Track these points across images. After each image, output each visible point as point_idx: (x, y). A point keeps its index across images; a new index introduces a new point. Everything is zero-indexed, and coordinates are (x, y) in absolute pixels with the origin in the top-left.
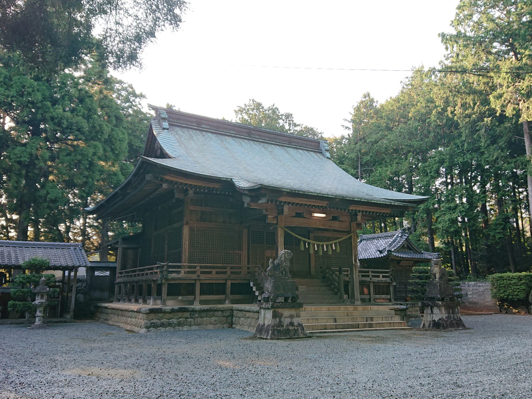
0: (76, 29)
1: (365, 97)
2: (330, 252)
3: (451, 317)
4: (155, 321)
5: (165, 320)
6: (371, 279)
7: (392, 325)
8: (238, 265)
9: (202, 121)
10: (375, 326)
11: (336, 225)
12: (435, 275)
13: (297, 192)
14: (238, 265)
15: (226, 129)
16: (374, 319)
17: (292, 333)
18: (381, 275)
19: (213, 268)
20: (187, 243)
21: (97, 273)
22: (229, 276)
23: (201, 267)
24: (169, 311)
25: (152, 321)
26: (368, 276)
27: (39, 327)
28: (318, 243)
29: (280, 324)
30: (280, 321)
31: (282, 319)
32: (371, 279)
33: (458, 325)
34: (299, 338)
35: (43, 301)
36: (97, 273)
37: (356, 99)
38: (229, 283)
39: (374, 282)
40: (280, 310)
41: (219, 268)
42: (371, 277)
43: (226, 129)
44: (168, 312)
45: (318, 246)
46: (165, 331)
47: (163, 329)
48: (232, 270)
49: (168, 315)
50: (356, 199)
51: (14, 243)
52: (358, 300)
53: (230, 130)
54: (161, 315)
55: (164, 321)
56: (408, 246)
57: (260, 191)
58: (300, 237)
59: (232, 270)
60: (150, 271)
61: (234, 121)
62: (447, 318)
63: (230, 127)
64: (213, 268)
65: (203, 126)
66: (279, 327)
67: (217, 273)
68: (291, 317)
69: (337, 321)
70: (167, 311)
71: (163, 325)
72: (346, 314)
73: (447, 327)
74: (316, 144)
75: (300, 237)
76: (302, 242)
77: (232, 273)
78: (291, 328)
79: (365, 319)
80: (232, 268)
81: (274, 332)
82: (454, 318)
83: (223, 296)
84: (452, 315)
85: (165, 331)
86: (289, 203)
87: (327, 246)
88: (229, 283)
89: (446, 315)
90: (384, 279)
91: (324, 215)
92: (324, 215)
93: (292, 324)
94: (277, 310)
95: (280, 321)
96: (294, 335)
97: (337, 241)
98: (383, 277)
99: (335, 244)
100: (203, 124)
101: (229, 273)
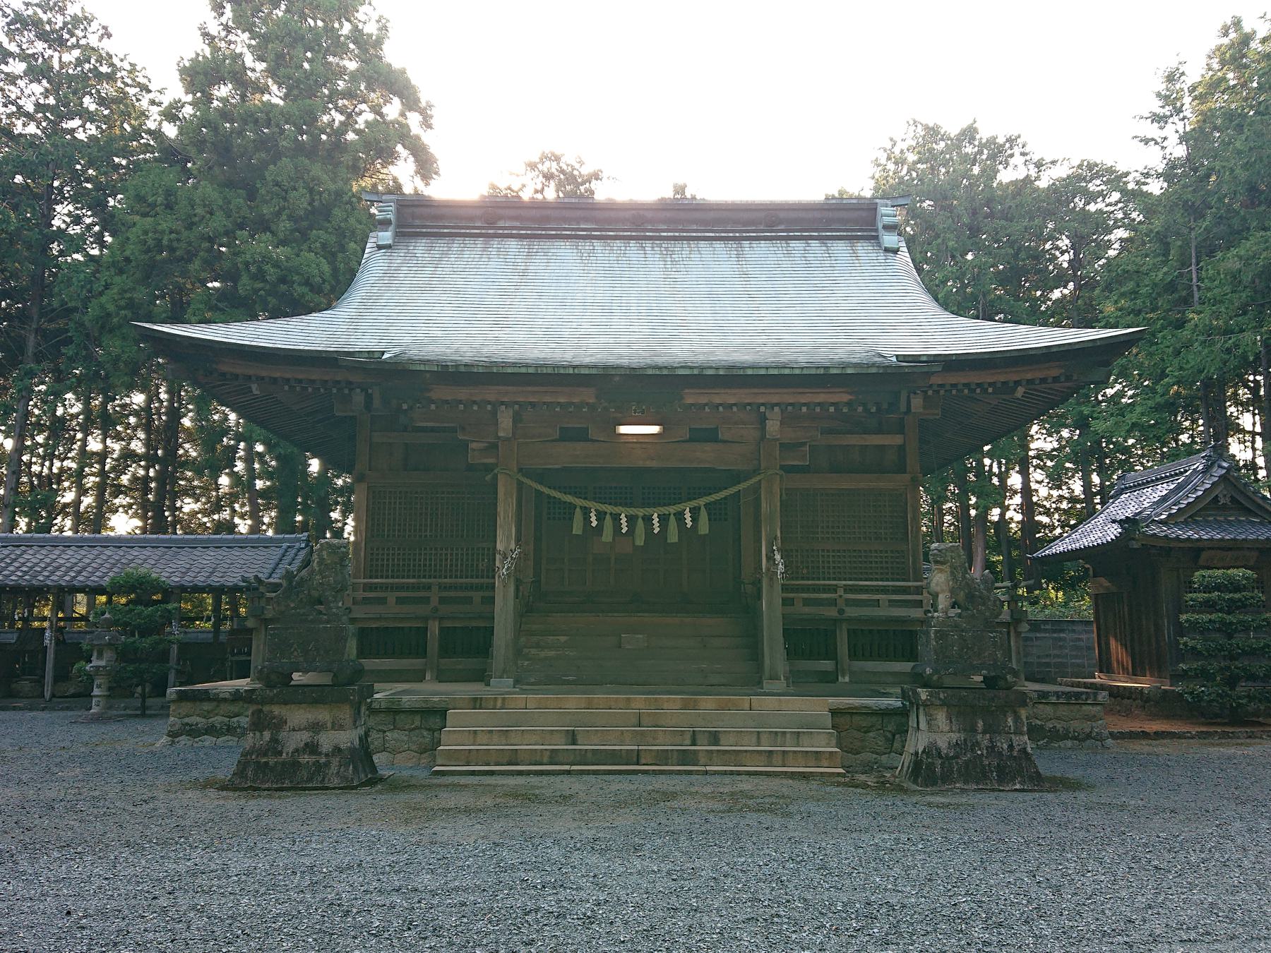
1: (1226, 34)
2: (673, 537)
4: (194, 720)
5: (220, 718)
6: (841, 612)
7: (777, 759)
8: (477, 581)
9: (501, 212)
10: (702, 761)
11: (705, 455)
12: (935, 596)
13: (462, 369)
14: (477, 581)
15: (565, 220)
17: (305, 774)
18: (392, 597)
22: (436, 610)
24: (227, 695)
25: (186, 720)
27: (99, 719)
28: (632, 511)
29: (274, 747)
30: (274, 740)
31: (283, 735)
33: (1013, 772)
34: (327, 788)
35: (102, 663)
38: (434, 628)
39: (850, 620)
40: (276, 710)
43: (565, 220)
44: (225, 700)
45: (601, 516)
46: (215, 747)
47: (208, 740)
49: (225, 708)
50: (849, 371)
51: (209, 541)
52: (774, 677)
53: (578, 221)
54: (207, 706)
55: (217, 720)
56: (1233, 499)
58: (569, 498)
59: (445, 594)
61: (526, 196)
63: (579, 213)
65: (501, 224)
66: (265, 755)
67: (400, 601)
68: (316, 727)
69: (580, 738)
70: (221, 696)
71: (211, 730)
72: (635, 721)
73: (947, 778)
74: (864, 214)
75: (569, 498)
76: (578, 509)
77: (443, 600)
78: (305, 759)
80: (443, 587)
81: (244, 769)
83: (416, 663)
84: (984, 740)
85: (215, 747)
86: (533, 405)
87: (631, 520)
88: (434, 628)
90: (807, 610)
91: (654, 429)
92: (654, 429)
93: (312, 748)
94: (266, 708)
95: (274, 740)
96: (310, 780)
97: (702, 502)
99: (695, 512)
100: (501, 218)
101: (434, 601)
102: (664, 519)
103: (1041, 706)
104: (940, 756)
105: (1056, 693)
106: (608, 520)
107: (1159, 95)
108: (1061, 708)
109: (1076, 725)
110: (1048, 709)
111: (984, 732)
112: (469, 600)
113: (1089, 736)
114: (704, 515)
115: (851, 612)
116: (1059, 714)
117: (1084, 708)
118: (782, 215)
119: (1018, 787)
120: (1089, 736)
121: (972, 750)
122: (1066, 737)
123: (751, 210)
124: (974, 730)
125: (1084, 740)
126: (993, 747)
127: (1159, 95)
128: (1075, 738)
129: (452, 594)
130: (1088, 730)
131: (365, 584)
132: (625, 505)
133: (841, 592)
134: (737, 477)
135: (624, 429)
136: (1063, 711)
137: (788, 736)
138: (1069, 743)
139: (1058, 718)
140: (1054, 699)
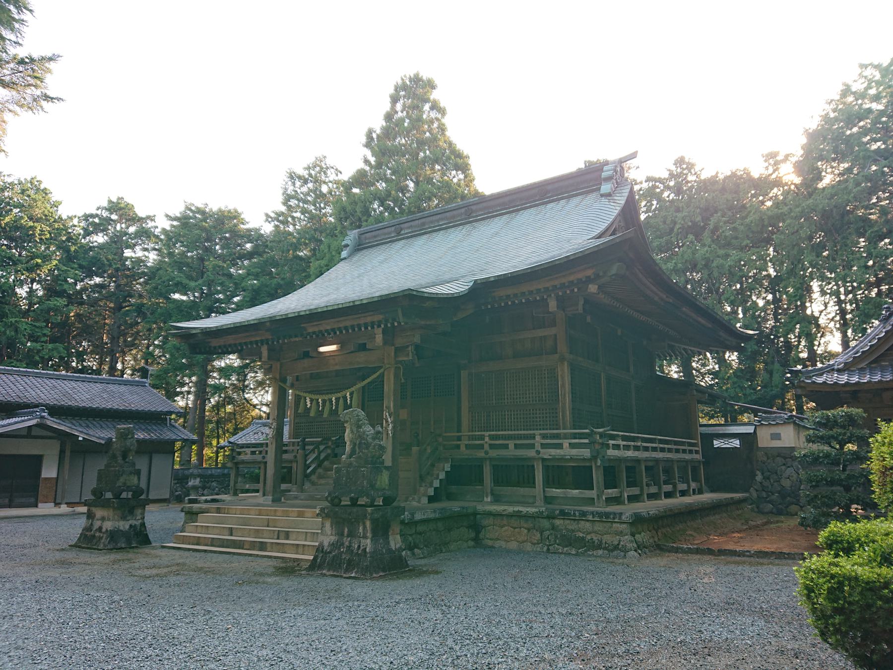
0: (22, 292)
3: (343, 544)
6: (487, 453)
7: (301, 549)
10: (269, 549)
16: (290, 535)
18: (511, 444)
19: (510, 437)
20: (568, 387)
21: (717, 443)
23: (492, 438)
26: (532, 446)
32: (538, 452)
36: (717, 443)
37: (319, 155)
39: (491, 459)
41: (520, 437)
42: (486, 447)
45: (312, 400)
48: (531, 442)
57: (482, 290)
59: (531, 442)
60: (625, 443)
62: (331, 545)
64: (510, 437)
72: (266, 524)
79: (276, 533)
82: (349, 547)
89: (333, 538)
90: (574, 452)
92: (322, 349)
97: (353, 389)
98: (572, 446)
102: (324, 401)
103: (583, 522)
104: (322, 552)
105: (592, 513)
106: (314, 402)
107: (60, 203)
108: (597, 524)
109: (607, 538)
110: (588, 524)
111: (348, 536)
112: (506, 447)
113: (616, 548)
114: (355, 395)
115: (494, 453)
116: (596, 528)
117: (614, 525)
118: (549, 187)
119: (353, 575)
120: (616, 548)
121: (339, 549)
122: (599, 547)
123: (530, 189)
124: (342, 535)
125: (612, 551)
126: (350, 546)
127: (60, 203)
128: (605, 548)
129: (549, 441)
130: (616, 543)
131: (571, 433)
132: (309, 392)
133: (487, 439)
134: (374, 370)
135: (322, 349)
136: (598, 527)
137: (309, 535)
138: (600, 552)
139: (595, 532)
140: (590, 518)
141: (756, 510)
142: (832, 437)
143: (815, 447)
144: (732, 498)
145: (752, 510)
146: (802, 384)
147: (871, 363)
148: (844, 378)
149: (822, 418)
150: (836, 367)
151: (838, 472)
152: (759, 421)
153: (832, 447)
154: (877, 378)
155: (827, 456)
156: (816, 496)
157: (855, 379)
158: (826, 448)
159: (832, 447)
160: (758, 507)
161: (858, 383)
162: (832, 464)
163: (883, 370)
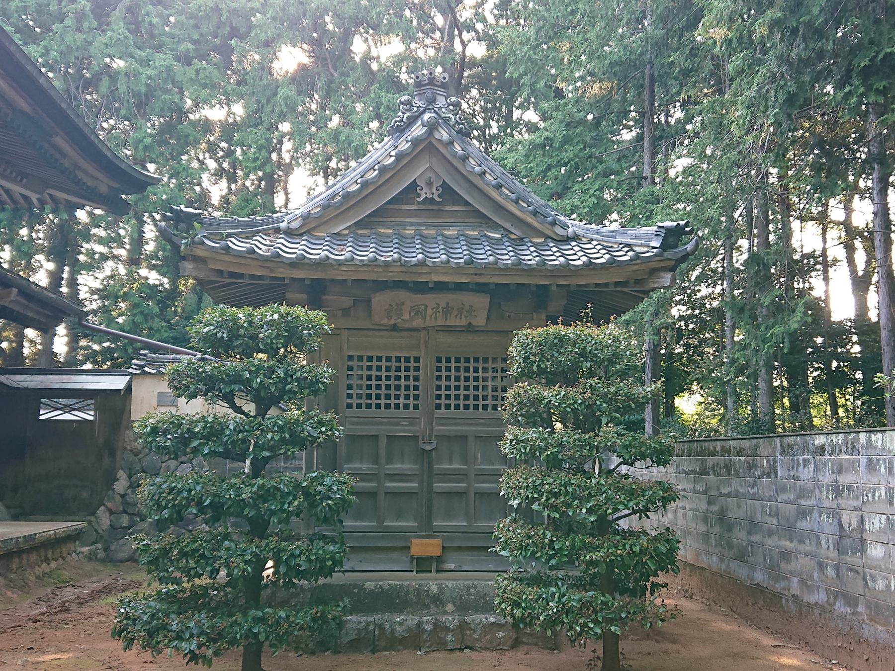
141: (101, 555)
142: (236, 378)
143: (193, 408)
144: (29, 538)
145: (91, 557)
146: (200, 252)
147: (359, 224)
148: (292, 249)
149: (220, 325)
150: (283, 225)
151: (240, 481)
152: (141, 367)
153: (239, 410)
154: (367, 254)
155: (214, 431)
156: (165, 552)
157: (318, 253)
158: (222, 409)
159: (239, 410)
160: (106, 550)
161: (324, 263)
162: (227, 455)
163: (381, 241)
